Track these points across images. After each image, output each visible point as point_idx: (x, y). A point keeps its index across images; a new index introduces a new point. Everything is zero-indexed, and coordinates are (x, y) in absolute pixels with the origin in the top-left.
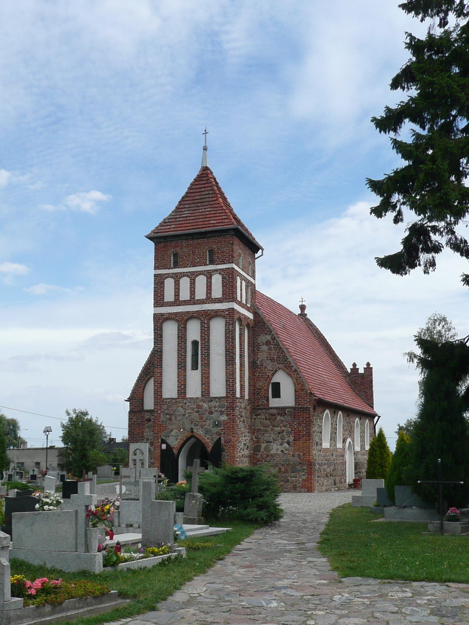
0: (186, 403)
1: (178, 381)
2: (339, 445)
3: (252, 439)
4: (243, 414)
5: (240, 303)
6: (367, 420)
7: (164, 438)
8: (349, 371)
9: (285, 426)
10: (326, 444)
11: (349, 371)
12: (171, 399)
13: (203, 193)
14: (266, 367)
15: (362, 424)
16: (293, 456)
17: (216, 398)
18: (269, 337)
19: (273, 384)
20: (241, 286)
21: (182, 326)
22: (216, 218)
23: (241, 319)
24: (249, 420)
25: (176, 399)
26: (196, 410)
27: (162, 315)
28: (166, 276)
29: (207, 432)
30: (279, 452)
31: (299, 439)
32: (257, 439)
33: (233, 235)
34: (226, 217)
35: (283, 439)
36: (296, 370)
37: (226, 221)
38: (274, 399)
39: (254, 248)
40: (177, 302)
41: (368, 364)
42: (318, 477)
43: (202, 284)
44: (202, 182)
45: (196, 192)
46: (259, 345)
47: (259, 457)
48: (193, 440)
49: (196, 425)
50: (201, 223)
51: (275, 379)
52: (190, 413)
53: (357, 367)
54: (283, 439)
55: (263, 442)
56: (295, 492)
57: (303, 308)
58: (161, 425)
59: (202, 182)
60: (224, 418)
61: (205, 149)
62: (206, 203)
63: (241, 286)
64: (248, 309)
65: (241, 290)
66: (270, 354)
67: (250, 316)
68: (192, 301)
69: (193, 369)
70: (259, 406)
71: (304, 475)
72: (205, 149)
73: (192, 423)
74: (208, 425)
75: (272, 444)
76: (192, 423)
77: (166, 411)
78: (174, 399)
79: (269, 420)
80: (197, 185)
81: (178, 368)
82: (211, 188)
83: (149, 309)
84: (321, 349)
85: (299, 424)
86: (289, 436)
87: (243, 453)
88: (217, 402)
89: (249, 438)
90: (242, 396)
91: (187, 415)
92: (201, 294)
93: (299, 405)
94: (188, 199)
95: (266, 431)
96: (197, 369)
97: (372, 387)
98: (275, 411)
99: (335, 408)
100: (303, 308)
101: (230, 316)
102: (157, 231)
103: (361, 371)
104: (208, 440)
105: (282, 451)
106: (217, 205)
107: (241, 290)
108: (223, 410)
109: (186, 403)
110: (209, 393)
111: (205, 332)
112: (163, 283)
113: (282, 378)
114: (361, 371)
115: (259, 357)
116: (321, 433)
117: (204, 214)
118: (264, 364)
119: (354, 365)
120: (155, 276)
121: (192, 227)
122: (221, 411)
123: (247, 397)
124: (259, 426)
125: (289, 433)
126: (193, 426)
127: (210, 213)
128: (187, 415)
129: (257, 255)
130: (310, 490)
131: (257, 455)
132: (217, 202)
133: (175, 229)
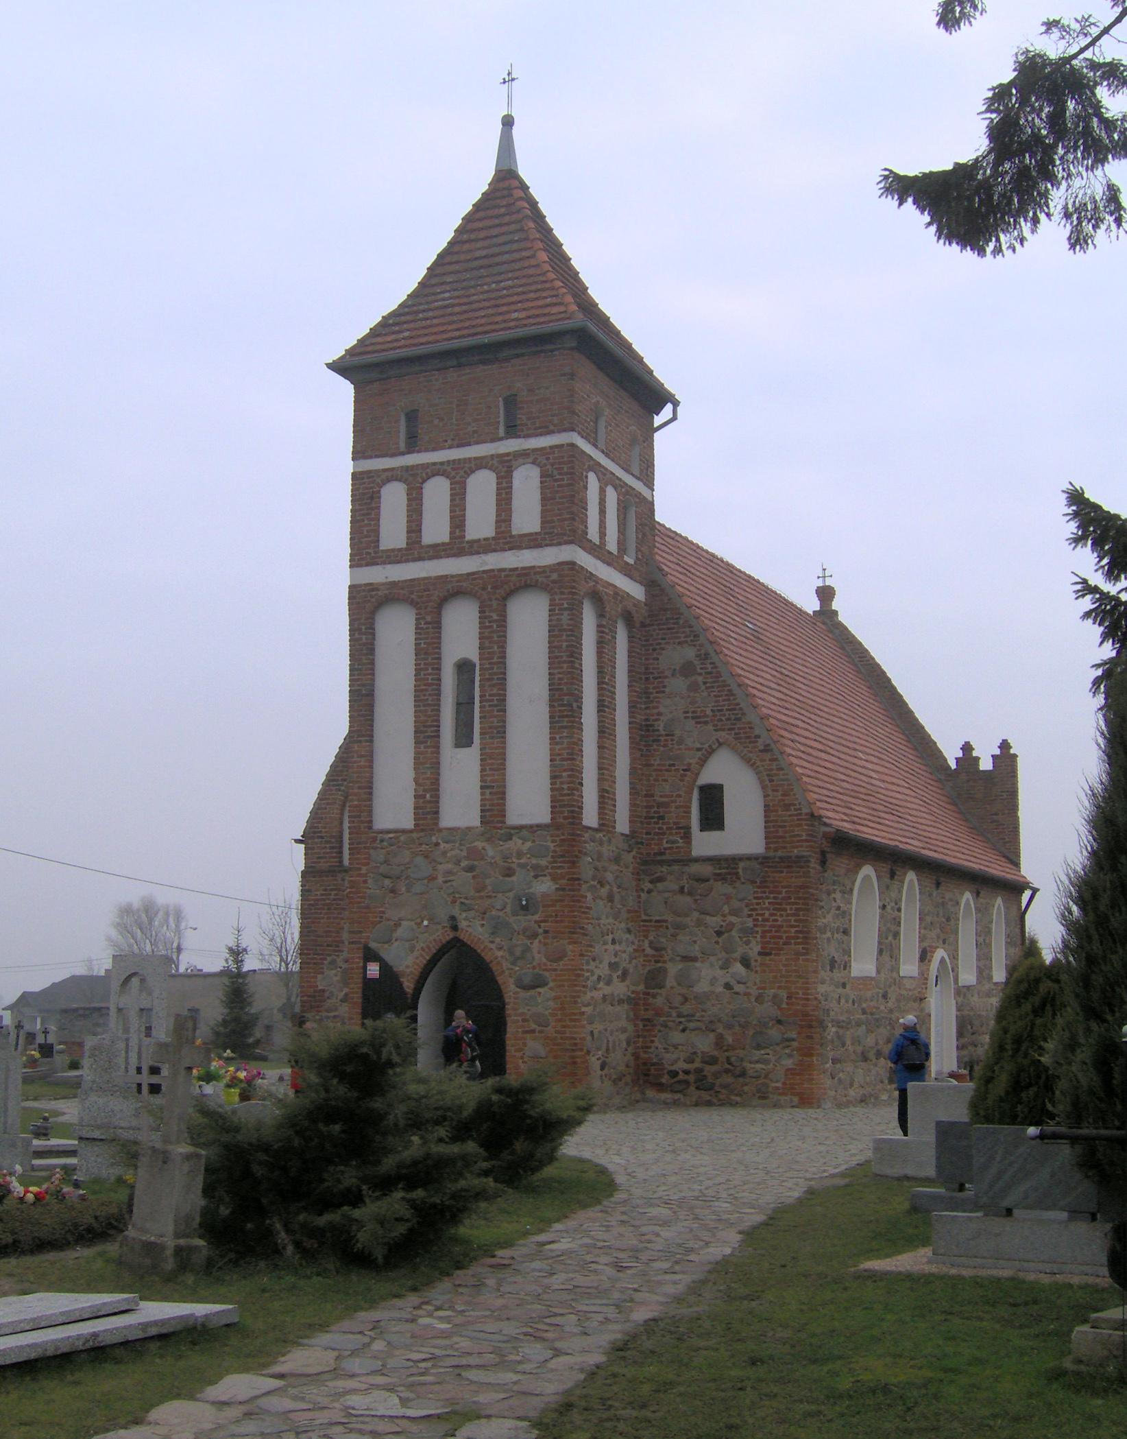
0: (437, 844)
1: (416, 780)
2: (909, 968)
3: (639, 950)
4: (610, 877)
5: (597, 550)
6: (999, 901)
7: (373, 945)
8: (953, 766)
9: (734, 913)
10: (864, 965)
11: (953, 766)
12: (396, 831)
13: (495, 240)
15: (983, 911)
16: (759, 999)
17: (521, 828)
18: (690, 653)
20: (602, 502)
21: (429, 618)
22: (526, 305)
23: (600, 596)
25: (411, 831)
26: (464, 863)
27: (372, 588)
28: (384, 476)
29: (497, 928)
30: (720, 989)
32: (657, 949)
33: (572, 349)
34: (554, 300)
36: (767, 749)
37: (555, 310)
38: (705, 834)
39: (644, 395)
40: (415, 550)
41: (1005, 745)
42: (835, 1061)
43: (491, 498)
44: (496, 211)
45: (477, 240)
47: (659, 1001)
49: (468, 908)
50: (483, 321)
51: (708, 776)
52: (450, 872)
53: (975, 754)
55: (672, 960)
56: (763, 1106)
57: (825, 594)
58: (367, 907)
59: (496, 211)
60: (544, 887)
62: (504, 268)
63: (602, 502)
64: (627, 571)
65: (602, 512)
67: (636, 591)
68: (458, 545)
70: (662, 854)
71: (790, 1056)
72: (508, 122)
73: (454, 902)
75: (698, 964)
76: (454, 902)
77: (383, 869)
78: (404, 831)
79: (690, 894)
80: (480, 220)
82: (518, 226)
86: (747, 943)
87: (607, 990)
88: (524, 840)
89: (630, 949)
90: (606, 824)
91: (440, 880)
92: (480, 524)
93: (776, 850)
94: (455, 258)
95: (680, 927)
96: (469, 743)
97: (1014, 808)
98: (707, 870)
100: (825, 594)
101: (565, 587)
102: (362, 350)
103: (986, 764)
104: (500, 953)
105: (728, 986)
106: (531, 271)
107: (602, 512)
108: (543, 862)
109: (437, 844)
110: (502, 814)
111: (494, 634)
114: (986, 764)
115: (662, 709)
116: (846, 932)
117: (493, 295)
118: (678, 733)
119: (967, 748)
121: (457, 333)
122: (536, 867)
123: (622, 824)
125: (747, 932)
126: (456, 911)
127: (511, 291)
128: (440, 880)
129: (658, 420)
130: (806, 1100)
131: (654, 996)
132: (533, 262)
133: (412, 341)
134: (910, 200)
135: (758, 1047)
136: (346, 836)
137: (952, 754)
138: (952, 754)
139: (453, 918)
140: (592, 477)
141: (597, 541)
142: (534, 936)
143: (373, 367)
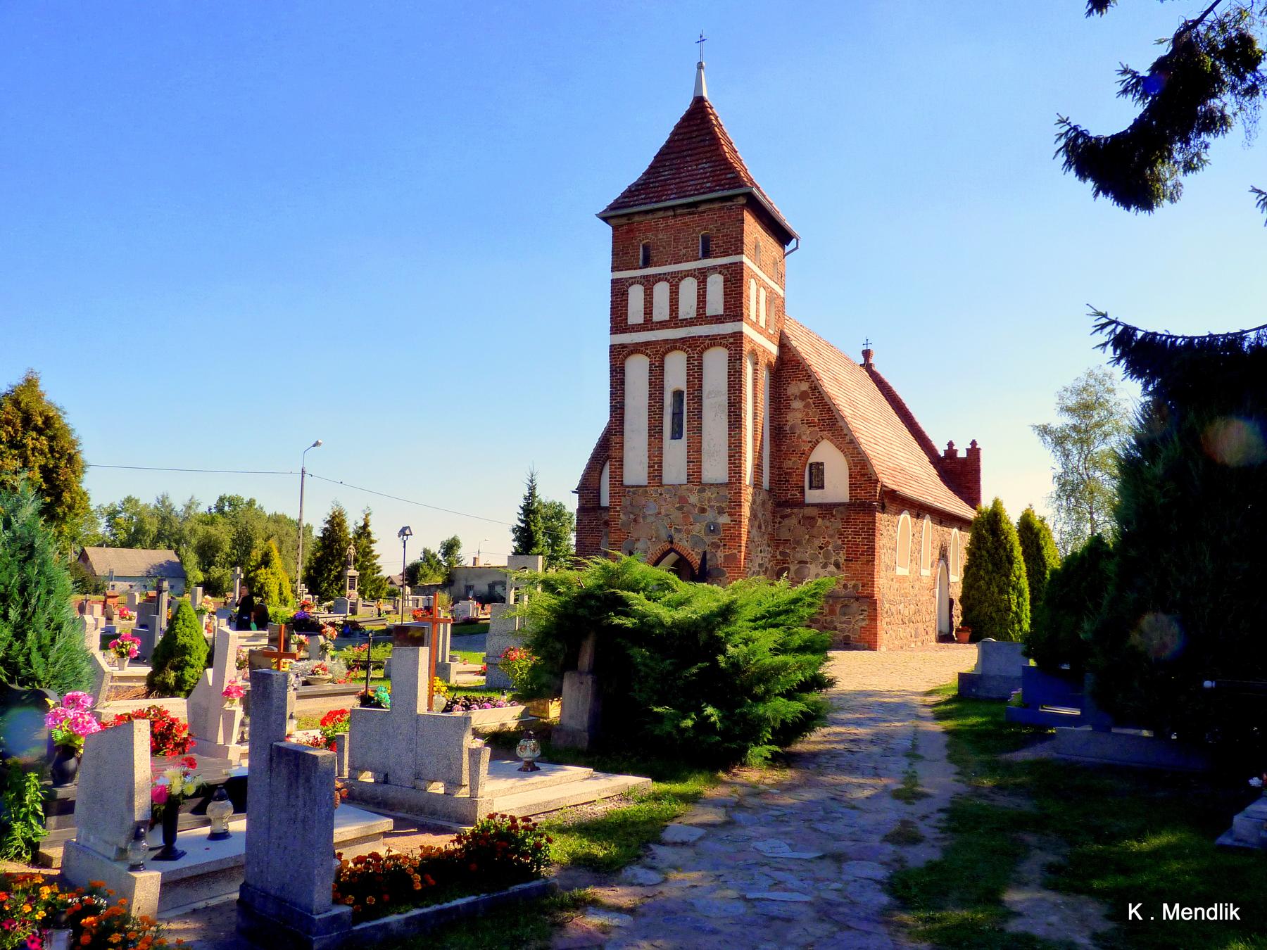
5: (755, 325)
8: (942, 454)
11: (942, 454)
14: (800, 437)
18: (804, 386)
19: (811, 465)
20: (758, 296)
24: (771, 524)
27: (623, 346)
35: (827, 556)
40: (649, 324)
41: (974, 443)
46: (788, 399)
51: (813, 459)
54: (827, 556)
61: (700, 66)
63: (758, 296)
65: (758, 303)
66: (807, 414)
68: (674, 321)
69: (673, 438)
72: (700, 66)
74: (698, 529)
83: (601, 339)
85: (856, 533)
92: (688, 307)
99: (920, 509)
103: (962, 454)
107: (758, 303)
114: (962, 454)
119: (951, 444)
120: (614, 282)
124: (785, 535)
125: (837, 549)
135: (845, 614)
136: (690, 200)
137: (941, 450)
138: (941, 450)
139: (670, 536)
140: (753, 281)
141: (754, 319)
142: (718, 547)
143: (622, 215)
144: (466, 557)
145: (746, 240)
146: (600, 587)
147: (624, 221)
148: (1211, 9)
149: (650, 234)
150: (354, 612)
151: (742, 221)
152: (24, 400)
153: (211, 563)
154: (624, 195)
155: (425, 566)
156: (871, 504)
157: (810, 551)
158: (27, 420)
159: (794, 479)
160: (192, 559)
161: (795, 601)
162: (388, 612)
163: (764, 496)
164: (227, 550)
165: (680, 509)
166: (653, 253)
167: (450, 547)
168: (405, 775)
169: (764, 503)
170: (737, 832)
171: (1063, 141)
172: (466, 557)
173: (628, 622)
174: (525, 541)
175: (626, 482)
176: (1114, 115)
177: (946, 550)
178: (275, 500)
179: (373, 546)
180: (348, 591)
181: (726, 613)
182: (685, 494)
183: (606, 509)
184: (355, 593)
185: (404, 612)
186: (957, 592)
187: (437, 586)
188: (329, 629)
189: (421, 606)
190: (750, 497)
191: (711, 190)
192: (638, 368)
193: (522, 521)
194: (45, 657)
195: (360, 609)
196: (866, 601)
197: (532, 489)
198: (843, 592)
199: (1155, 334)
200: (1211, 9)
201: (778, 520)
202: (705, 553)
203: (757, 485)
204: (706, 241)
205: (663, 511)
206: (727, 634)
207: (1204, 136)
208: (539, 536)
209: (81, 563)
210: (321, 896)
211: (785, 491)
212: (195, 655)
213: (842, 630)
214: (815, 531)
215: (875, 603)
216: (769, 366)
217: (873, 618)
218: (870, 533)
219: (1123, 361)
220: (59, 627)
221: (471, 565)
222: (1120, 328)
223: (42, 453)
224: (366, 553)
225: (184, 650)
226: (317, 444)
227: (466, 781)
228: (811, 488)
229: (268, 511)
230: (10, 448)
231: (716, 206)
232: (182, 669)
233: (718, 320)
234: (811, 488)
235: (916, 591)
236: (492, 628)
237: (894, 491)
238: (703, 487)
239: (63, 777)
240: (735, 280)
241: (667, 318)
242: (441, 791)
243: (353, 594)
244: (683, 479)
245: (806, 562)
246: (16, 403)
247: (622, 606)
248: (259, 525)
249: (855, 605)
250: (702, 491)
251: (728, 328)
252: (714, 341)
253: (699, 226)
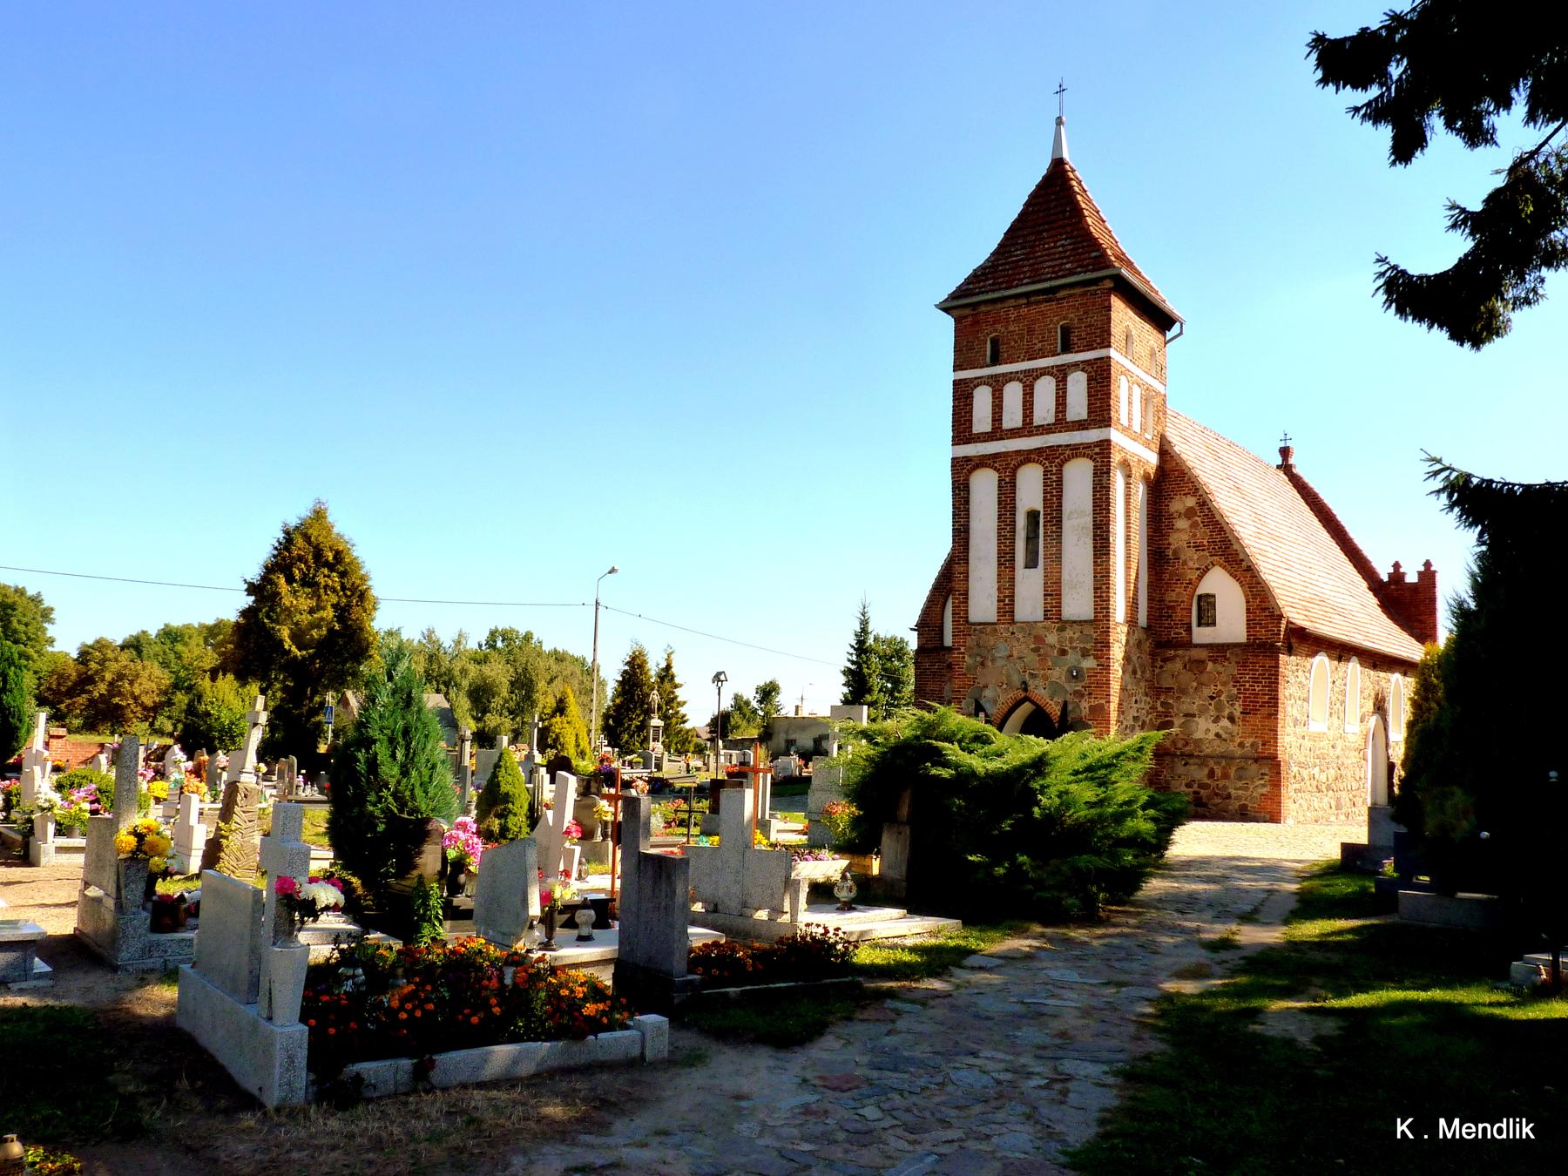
3: (1153, 708)
5: (1126, 430)
8: (1385, 579)
10: (1319, 724)
11: (1385, 579)
14: (1185, 563)
16: (1241, 745)
18: (1191, 502)
19: (1200, 597)
20: (1130, 395)
27: (967, 459)
31: (1255, 711)
35: (1219, 708)
40: (997, 433)
41: (1428, 564)
46: (1171, 517)
48: (1026, 708)
49: (1033, 676)
51: (1203, 589)
54: (1219, 708)
61: (1059, 122)
63: (1130, 395)
64: (1147, 444)
66: (1194, 535)
69: (1027, 567)
72: (1059, 122)
74: (1058, 674)
81: (1000, 565)
83: (941, 451)
84: (1324, 535)
85: (1255, 680)
92: (1044, 411)
96: (1035, 566)
98: (1203, 654)
99: (1342, 651)
103: (1412, 578)
112: (970, 397)
113: (1220, 584)
114: (1412, 578)
116: (1306, 700)
119: (1397, 566)
120: (956, 383)
125: (1232, 699)
134: (1436, 122)
135: (1240, 778)
136: (1046, 285)
139: (1024, 683)
141: (1126, 424)
142: (1082, 696)
144: (787, 704)
145: (1113, 331)
146: (917, 738)
147: (967, 311)
148: (1546, 142)
149: (998, 326)
150: (659, 767)
151: (1109, 308)
152: (313, 532)
153: (485, 711)
154: (968, 281)
155: (737, 715)
156: (1272, 645)
157: (1198, 702)
158: (318, 553)
159: (1179, 613)
160: (464, 703)
161: (1117, 756)
162: (698, 769)
163: (1139, 635)
164: (505, 693)
165: (1034, 650)
166: (1003, 348)
167: (768, 693)
168: (733, 904)
169: (1139, 644)
170: (1037, 964)
171: (1382, 281)
172: (787, 704)
173: (946, 773)
174: (858, 686)
175: (973, 618)
176: (1439, 251)
177: (1383, 699)
178: (559, 633)
179: (678, 692)
180: (652, 744)
181: (1040, 765)
182: (1042, 632)
183: (950, 649)
184: (659, 746)
185: (720, 763)
186: (1398, 753)
187: (753, 740)
188: (640, 783)
189: (734, 762)
190: (1123, 638)
191: (1072, 273)
192: (985, 485)
193: (853, 663)
194: (426, 792)
195: (665, 764)
196: (1269, 763)
197: (864, 623)
198: (1239, 752)
199: (1492, 481)
200: (1546, 142)
201: (1159, 663)
202: (1065, 703)
203: (1132, 621)
204: (1066, 332)
205: (1015, 654)
206: (1043, 786)
207: (1544, 272)
208: (876, 681)
209: (341, 708)
210: (679, 965)
211: (1165, 631)
212: (517, 804)
213: (1238, 798)
214: (1204, 678)
215: (1278, 765)
216: (1146, 477)
217: (1276, 784)
218: (1272, 680)
219: (1456, 509)
220: (434, 767)
221: (792, 714)
222: (1454, 474)
223: (334, 590)
224: (671, 700)
225: (507, 798)
226: (613, 571)
227: (787, 908)
228: (1199, 625)
229: (547, 647)
230: (303, 586)
231: (1078, 291)
232: (506, 817)
233: (1081, 425)
234: (1199, 625)
235: (1338, 751)
236: (814, 782)
237: (1303, 629)
238: (1064, 625)
239: (456, 888)
240: (1100, 377)
241: (1020, 424)
242: (765, 918)
243: (656, 748)
244: (1040, 616)
245: (1194, 716)
246: (307, 538)
247: (939, 758)
248: (541, 664)
249: (1254, 767)
250: (1062, 629)
251: (1093, 435)
252: (1076, 451)
253: (1054, 318)
